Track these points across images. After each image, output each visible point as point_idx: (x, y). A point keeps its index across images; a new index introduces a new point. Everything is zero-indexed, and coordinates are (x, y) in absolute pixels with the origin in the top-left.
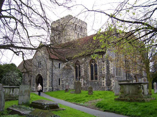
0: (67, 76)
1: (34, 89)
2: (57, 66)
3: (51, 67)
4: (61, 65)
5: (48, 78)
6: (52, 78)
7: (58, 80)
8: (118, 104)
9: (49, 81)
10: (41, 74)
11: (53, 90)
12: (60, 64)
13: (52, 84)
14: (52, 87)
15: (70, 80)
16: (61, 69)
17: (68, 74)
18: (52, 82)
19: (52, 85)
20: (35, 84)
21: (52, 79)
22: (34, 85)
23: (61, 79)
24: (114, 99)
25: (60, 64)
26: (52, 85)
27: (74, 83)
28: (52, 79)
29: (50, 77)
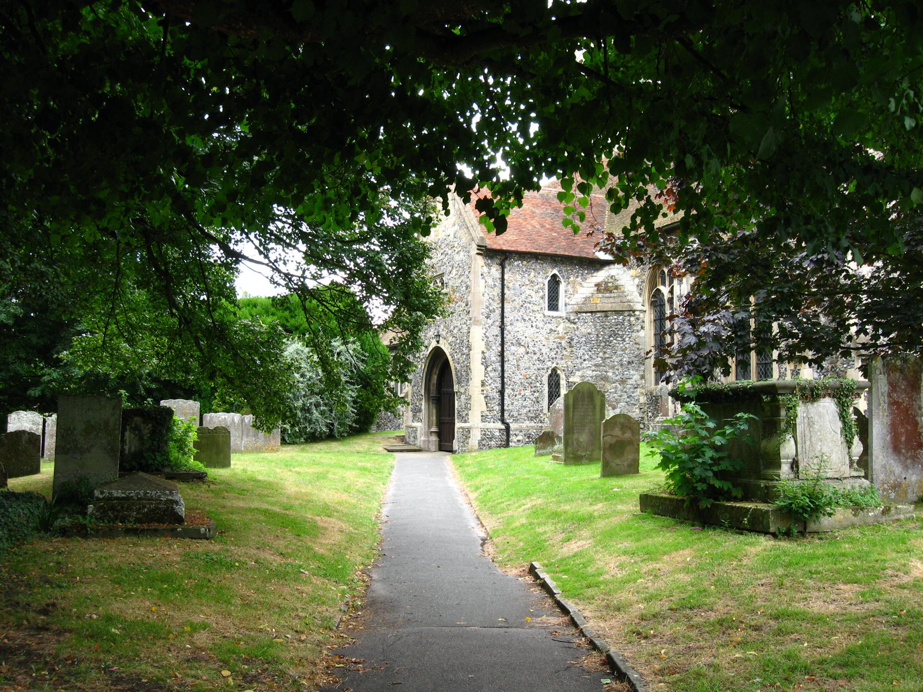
0: (604, 359)
1: (418, 435)
2: (538, 295)
3: (496, 305)
4: (562, 287)
5: (477, 372)
6: (503, 371)
7: (545, 380)
8: (667, 283)
9: (483, 384)
10: (447, 350)
11: (508, 441)
12: (554, 283)
13: (502, 404)
14: (503, 421)
15: (623, 382)
16: (562, 312)
17: (607, 343)
18: (502, 393)
19: (503, 411)
20: (423, 407)
21: (503, 377)
22: (420, 411)
23: (562, 376)
24: (633, 506)
25: (554, 283)
26: (503, 411)
27: (643, 400)
28: (503, 377)
29: (486, 363)
